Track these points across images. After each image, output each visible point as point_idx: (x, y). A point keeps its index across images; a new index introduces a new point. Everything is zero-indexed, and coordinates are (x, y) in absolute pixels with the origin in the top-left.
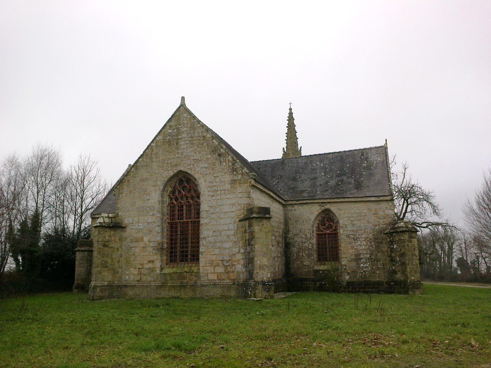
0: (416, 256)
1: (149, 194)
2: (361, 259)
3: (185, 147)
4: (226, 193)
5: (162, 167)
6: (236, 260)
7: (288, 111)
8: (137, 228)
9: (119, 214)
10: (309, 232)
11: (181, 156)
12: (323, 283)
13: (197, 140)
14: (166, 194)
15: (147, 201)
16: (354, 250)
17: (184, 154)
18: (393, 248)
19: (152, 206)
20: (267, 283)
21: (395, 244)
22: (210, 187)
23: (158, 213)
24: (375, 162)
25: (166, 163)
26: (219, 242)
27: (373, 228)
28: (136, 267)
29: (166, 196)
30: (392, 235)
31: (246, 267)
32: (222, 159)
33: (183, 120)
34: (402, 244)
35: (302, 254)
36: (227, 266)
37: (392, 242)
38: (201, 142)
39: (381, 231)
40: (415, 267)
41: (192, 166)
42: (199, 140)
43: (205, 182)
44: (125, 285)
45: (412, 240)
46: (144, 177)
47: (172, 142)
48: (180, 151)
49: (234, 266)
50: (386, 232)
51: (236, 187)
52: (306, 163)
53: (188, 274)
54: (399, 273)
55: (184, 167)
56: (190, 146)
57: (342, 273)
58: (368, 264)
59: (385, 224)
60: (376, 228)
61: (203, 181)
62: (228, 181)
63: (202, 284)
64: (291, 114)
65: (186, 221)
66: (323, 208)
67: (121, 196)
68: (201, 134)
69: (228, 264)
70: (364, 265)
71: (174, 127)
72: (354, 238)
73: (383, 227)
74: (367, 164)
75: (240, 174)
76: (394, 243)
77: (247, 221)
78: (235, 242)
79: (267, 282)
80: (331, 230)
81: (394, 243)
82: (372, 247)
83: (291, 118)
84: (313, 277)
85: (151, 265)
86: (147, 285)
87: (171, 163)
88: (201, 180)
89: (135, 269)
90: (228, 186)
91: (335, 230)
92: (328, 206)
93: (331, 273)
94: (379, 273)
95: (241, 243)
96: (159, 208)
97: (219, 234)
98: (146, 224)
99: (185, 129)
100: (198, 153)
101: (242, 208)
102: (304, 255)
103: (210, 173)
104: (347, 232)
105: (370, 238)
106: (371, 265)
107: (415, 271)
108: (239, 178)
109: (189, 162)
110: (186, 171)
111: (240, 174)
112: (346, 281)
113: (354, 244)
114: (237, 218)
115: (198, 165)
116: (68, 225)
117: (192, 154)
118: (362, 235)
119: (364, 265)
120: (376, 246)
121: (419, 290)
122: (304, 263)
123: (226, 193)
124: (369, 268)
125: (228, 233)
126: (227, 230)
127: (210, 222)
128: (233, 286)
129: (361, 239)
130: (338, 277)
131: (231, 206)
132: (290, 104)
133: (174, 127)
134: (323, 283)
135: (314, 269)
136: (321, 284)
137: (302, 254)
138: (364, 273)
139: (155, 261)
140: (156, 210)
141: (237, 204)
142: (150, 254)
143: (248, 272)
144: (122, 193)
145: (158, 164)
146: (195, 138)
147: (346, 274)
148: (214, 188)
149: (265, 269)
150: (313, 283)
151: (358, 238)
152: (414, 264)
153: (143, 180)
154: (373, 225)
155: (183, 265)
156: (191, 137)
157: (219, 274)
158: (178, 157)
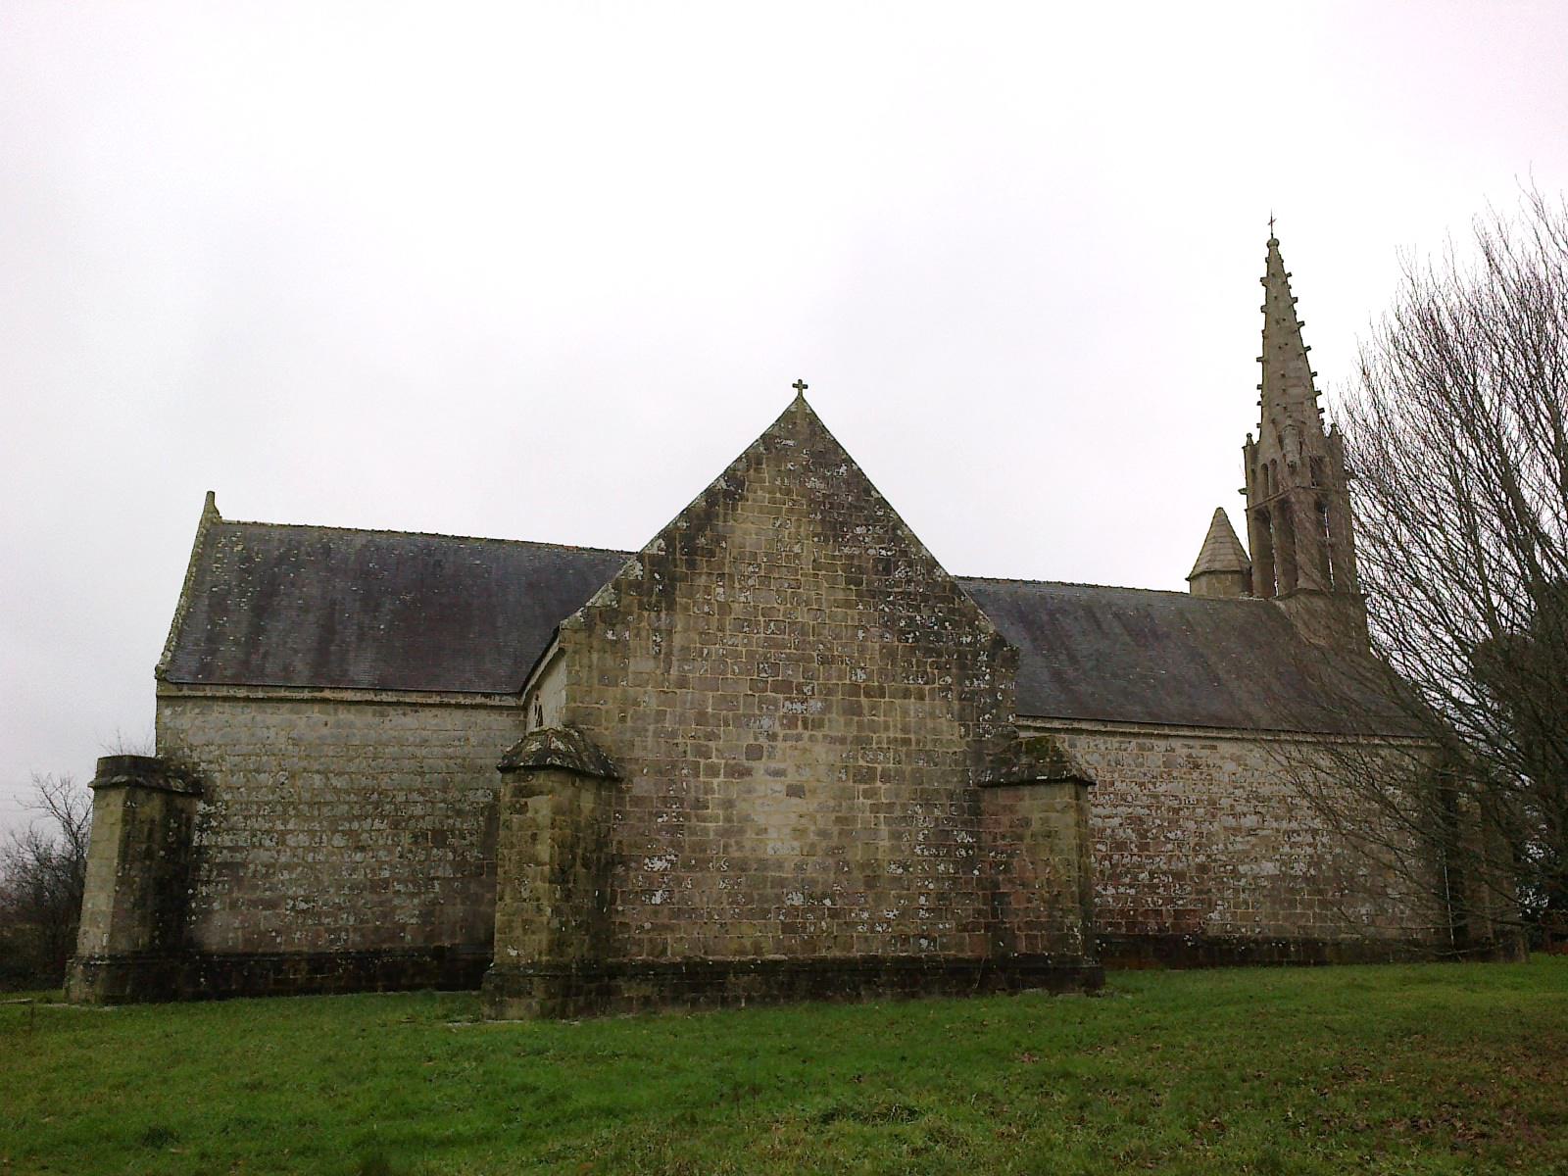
0: (538, 864)
7: (1266, 252)
45: (530, 801)
64: (1274, 261)
65: (974, 736)
83: (1276, 278)
107: (525, 922)
121: (526, 1001)
152: (525, 895)
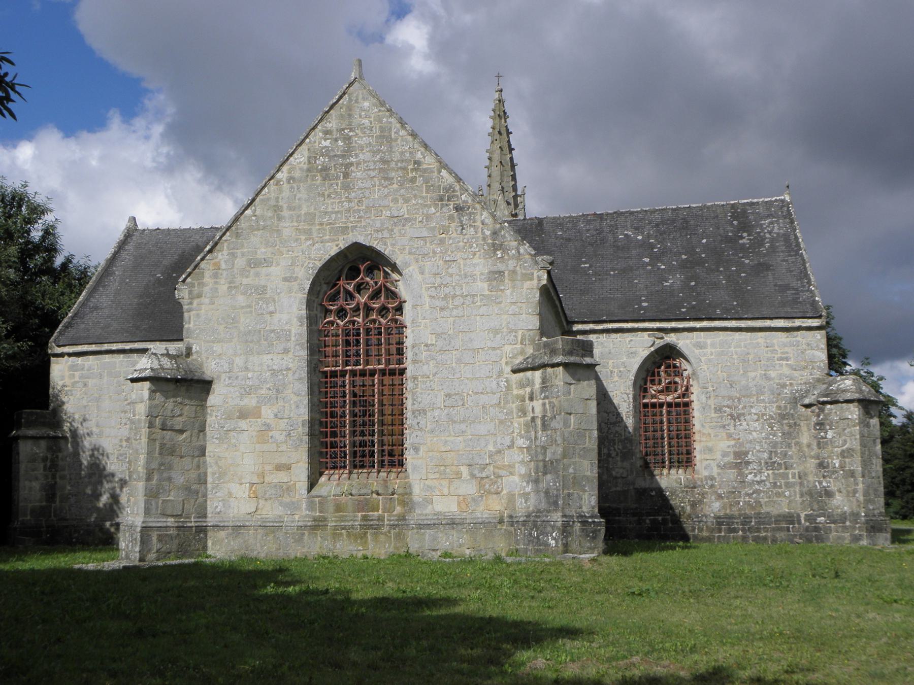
1: (274, 300)
2: (748, 463)
3: (368, 184)
4: (479, 304)
5: (308, 232)
6: (504, 466)
8: (243, 382)
9: (194, 347)
10: (626, 399)
11: (356, 207)
12: (660, 518)
13: (398, 168)
14: (316, 300)
15: (268, 317)
16: (733, 443)
17: (365, 202)
18: (826, 438)
19: (282, 330)
20: (590, 520)
21: (831, 429)
22: (436, 288)
23: (297, 347)
24: (768, 235)
25: (317, 222)
26: (461, 422)
27: (778, 392)
28: (244, 481)
29: (315, 305)
30: (822, 410)
31: (536, 481)
32: (465, 219)
33: (360, 116)
34: (848, 430)
35: (609, 450)
36: (482, 478)
37: (820, 425)
38: (410, 175)
39: (795, 398)
40: (875, 481)
41: (386, 234)
42: (405, 169)
43: (422, 273)
44: (218, 526)
46: (260, 256)
47: (333, 172)
48: (353, 194)
49: (499, 480)
50: (807, 401)
51: (502, 288)
52: (600, 232)
53: (381, 497)
54: (838, 497)
55: (367, 235)
56: (381, 185)
57: (703, 495)
58: (766, 474)
59: (805, 383)
60: (786, 391)
61: (417, 270)
62: (482, 274)
63: (420, 522)
66: (659, 343)
67: (195, 302)
68: (407, 155)
69: (484, 475)
70: (755, 476)
71: (336, 135)
72: (732, 415)
73: (801, 390)
74: (748, 239)
75: (513, 257)
76: (828, 427)
77: (538, 374)
78: (501, 422)
79: (590, 517)
80: (676, 395)
81: (828, 427)
82: (774, 436)
84: (634, 506)
85: (282, 477)
86: (275, 524)
87: (330, 224)
88: (411, 268)
89: (241, 484)
90: (482, 286)
91: (684, 396)
92: (671, 338)
93: (677, 496)
94: (790, 496)
95: (516, 425)
96: (300, 335)
97: (460, 404)
98: (268, 374)
99: (364, 141)
100: (401, 201)
101: (519, 339)
102: (614, 454)
103: (434, 252)
104: (716, 400)
105: (770, 415)
106: (771, 476)
108: (511, 268)
109: (378, 224)
110: (371, 245)
111: (513, 257)
112: (712, 515)
113: (732, 428)
114: (507, 363)
115: (403, 232)
116: (849, 396)
117: (386, 202)
118: (752, 407)
119: (755, 476)
120: (784, 434)
122: (614, 473)
123: (479, 304)
124: (767, 483)
125: (484, 399)
126: (482, 393)
127: (436, 373)
128: (499, 527)
129: (748, 417)
130: (693, 505)
131: (491, 335)
132: (498, 76)
133: (336, 135)
134: (660, 518)
135: (637, 486)
136: (654, 522)
137: (609, 450)
138: (754, 495)
139: (293, 466)
140: (293, 339)
141: (505, 330)
142: (280, 449)
143: (542, 495)
144: (199, 296)
145: (295, 224)
146: (393, 165)
147: (713, 498)
148: (447, 290)
149: (585, 486)
150: (636, 518)
151: (744, 414)
153: (255, 263)
154: (777, 385)
155: (366, 475)
156: (384, 161)
157: (461, 498)
158: (348, 210)
